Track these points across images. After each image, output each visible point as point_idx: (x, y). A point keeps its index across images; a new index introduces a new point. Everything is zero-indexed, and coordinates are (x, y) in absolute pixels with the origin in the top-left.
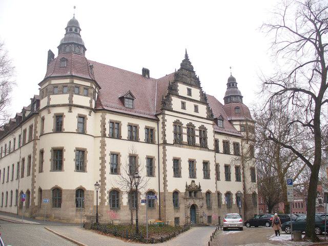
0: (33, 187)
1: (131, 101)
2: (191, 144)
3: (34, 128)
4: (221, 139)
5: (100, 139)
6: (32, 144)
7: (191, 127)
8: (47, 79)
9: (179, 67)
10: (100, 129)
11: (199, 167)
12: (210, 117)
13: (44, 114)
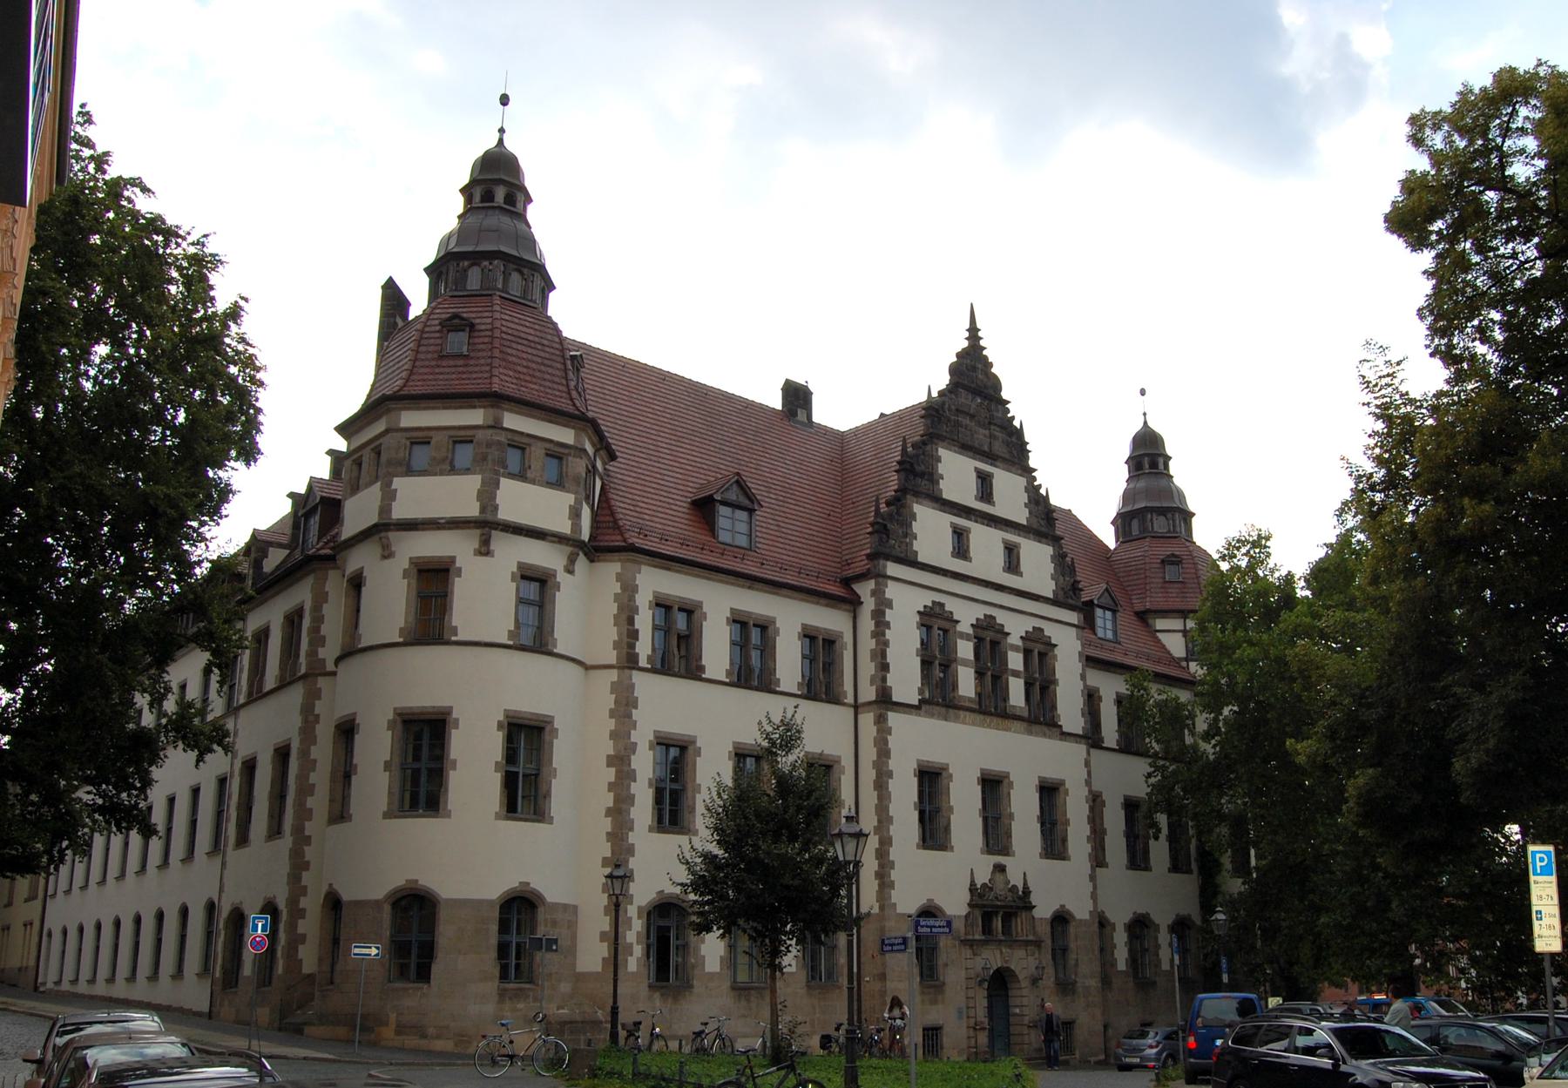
0: (297, 889)
1: (743, 515)
2: (991, 706)
3: (306, 623)
4: (1111, 687)
5: (613, 675)
6: (295, 695)
7: (989, 636)
8: (375, 407)
9: (941, 381)
10: (612, 634)
11: (1024, 806)
12: (1069, 595)
13: (361, 559)
